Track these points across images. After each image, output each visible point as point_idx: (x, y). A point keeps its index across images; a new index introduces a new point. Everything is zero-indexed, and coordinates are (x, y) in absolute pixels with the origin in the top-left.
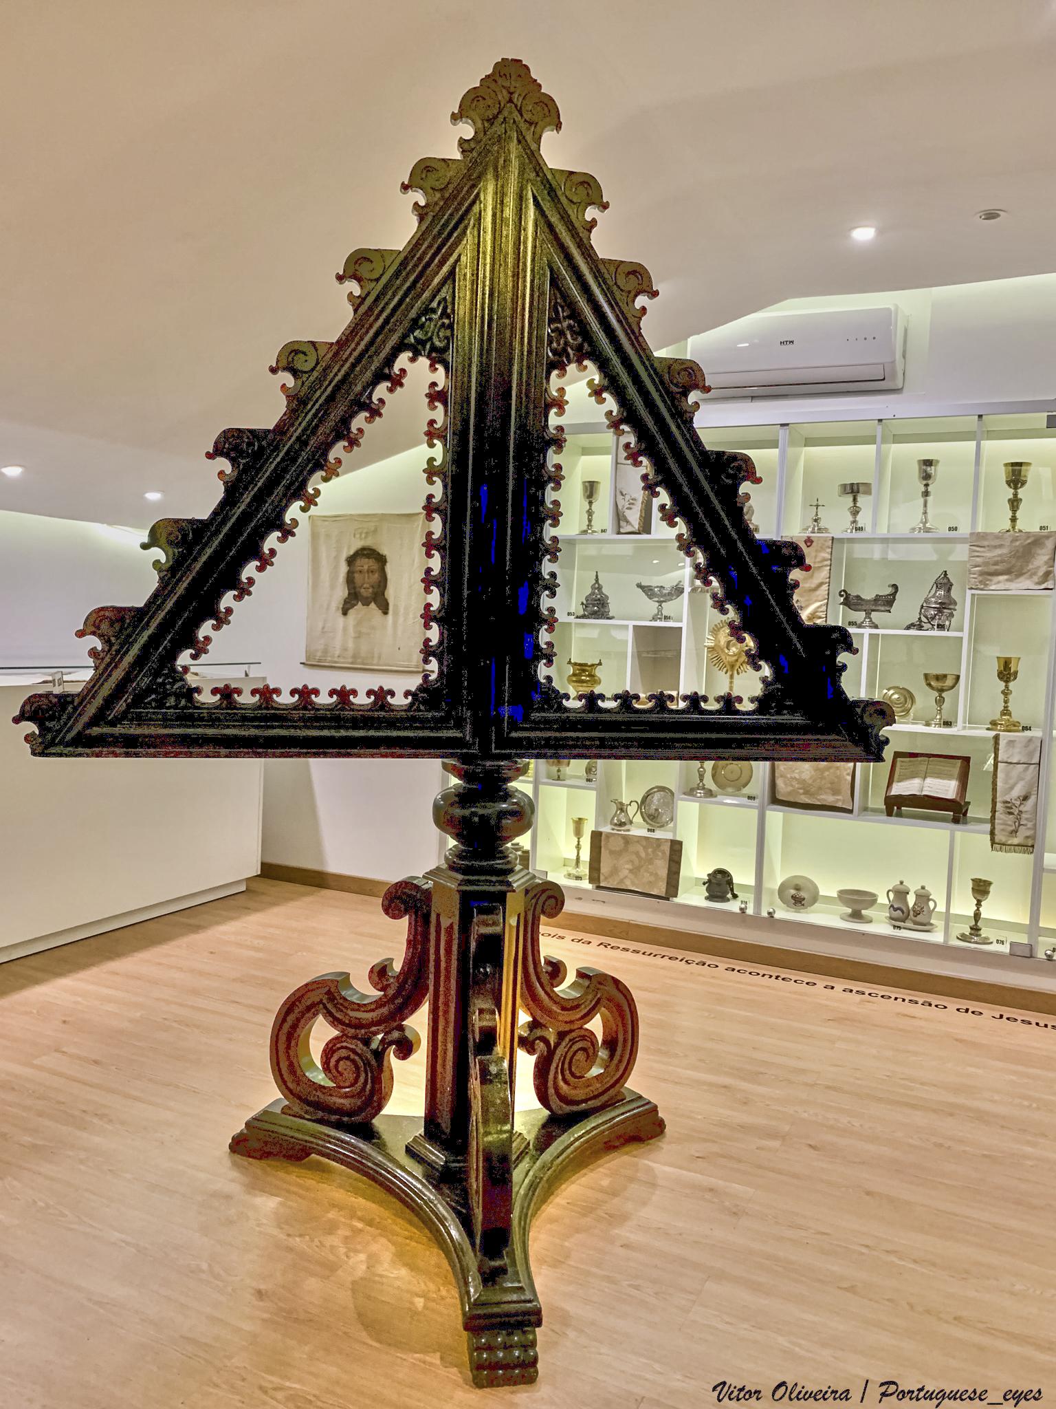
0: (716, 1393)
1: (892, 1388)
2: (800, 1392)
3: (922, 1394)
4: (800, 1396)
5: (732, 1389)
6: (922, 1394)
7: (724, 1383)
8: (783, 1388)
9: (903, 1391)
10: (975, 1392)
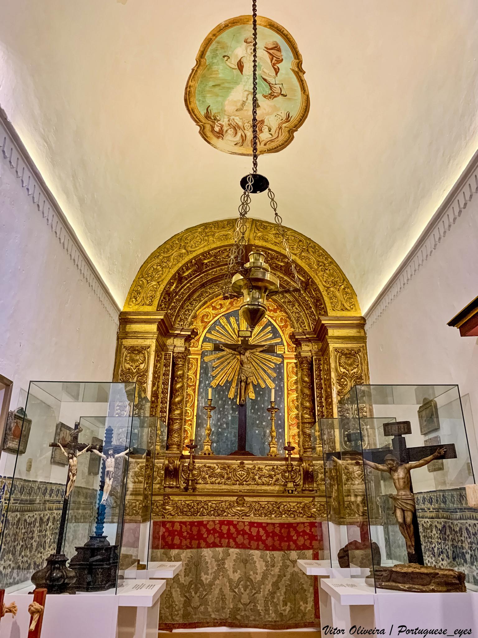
0: (325, 630)
1: (404, 629)
2: (362, 630)
3: (417, 631)
4: (362, 632)
5: (331, 629)
6: (417, 631)
7: (328, 626)
8: (354, 629)
9: (409, 630)
10: (441, 630)
